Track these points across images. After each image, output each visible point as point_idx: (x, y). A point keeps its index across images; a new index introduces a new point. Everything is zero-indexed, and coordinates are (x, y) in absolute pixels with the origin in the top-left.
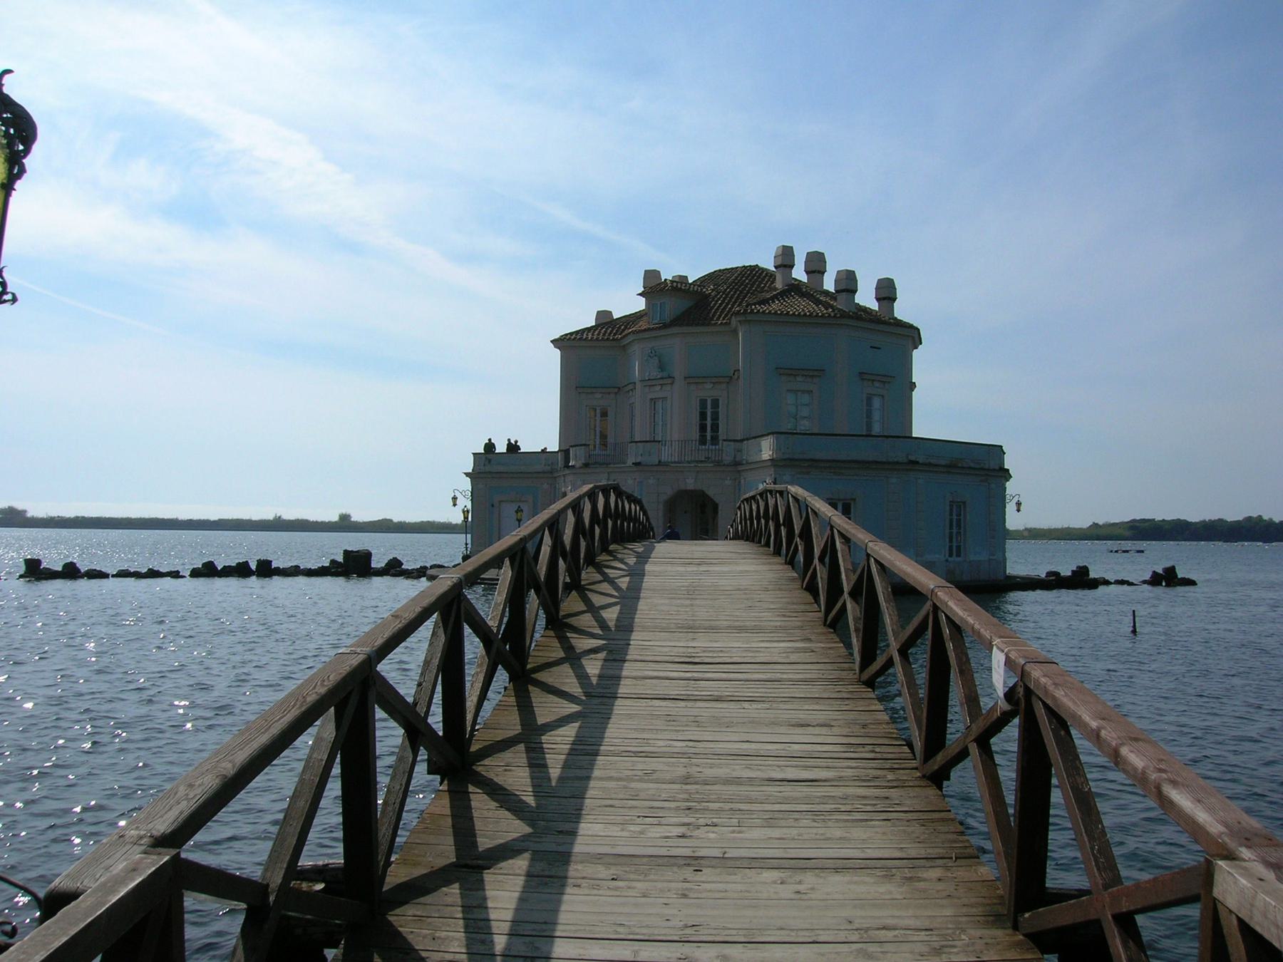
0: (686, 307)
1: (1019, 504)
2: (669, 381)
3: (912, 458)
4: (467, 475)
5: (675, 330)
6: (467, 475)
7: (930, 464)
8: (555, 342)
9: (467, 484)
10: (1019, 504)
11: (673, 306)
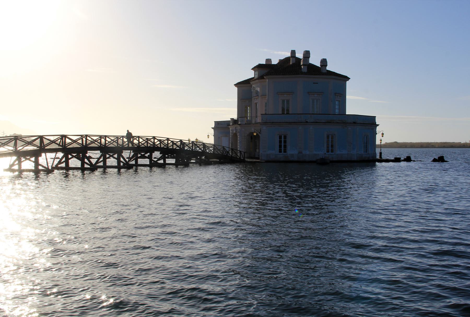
0: (266, 70)
1: (383, 134)
2: (257, 97)
3: (307, 121)
4: (212, 128)
5: (257, 81)
6: (212, 128)
7: (317, 122)
8: (236, 85)
9: (212, 131)
10: (383, 134)
11: (265, 71)
